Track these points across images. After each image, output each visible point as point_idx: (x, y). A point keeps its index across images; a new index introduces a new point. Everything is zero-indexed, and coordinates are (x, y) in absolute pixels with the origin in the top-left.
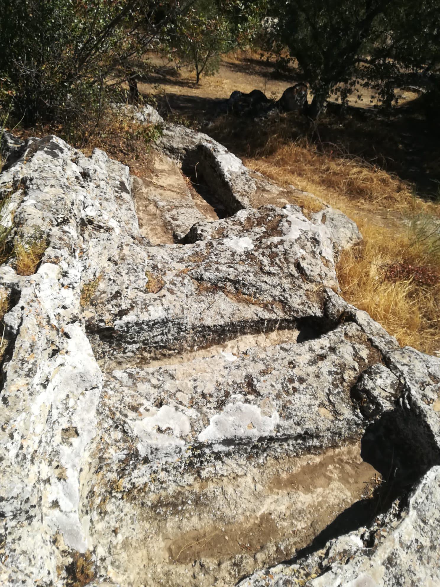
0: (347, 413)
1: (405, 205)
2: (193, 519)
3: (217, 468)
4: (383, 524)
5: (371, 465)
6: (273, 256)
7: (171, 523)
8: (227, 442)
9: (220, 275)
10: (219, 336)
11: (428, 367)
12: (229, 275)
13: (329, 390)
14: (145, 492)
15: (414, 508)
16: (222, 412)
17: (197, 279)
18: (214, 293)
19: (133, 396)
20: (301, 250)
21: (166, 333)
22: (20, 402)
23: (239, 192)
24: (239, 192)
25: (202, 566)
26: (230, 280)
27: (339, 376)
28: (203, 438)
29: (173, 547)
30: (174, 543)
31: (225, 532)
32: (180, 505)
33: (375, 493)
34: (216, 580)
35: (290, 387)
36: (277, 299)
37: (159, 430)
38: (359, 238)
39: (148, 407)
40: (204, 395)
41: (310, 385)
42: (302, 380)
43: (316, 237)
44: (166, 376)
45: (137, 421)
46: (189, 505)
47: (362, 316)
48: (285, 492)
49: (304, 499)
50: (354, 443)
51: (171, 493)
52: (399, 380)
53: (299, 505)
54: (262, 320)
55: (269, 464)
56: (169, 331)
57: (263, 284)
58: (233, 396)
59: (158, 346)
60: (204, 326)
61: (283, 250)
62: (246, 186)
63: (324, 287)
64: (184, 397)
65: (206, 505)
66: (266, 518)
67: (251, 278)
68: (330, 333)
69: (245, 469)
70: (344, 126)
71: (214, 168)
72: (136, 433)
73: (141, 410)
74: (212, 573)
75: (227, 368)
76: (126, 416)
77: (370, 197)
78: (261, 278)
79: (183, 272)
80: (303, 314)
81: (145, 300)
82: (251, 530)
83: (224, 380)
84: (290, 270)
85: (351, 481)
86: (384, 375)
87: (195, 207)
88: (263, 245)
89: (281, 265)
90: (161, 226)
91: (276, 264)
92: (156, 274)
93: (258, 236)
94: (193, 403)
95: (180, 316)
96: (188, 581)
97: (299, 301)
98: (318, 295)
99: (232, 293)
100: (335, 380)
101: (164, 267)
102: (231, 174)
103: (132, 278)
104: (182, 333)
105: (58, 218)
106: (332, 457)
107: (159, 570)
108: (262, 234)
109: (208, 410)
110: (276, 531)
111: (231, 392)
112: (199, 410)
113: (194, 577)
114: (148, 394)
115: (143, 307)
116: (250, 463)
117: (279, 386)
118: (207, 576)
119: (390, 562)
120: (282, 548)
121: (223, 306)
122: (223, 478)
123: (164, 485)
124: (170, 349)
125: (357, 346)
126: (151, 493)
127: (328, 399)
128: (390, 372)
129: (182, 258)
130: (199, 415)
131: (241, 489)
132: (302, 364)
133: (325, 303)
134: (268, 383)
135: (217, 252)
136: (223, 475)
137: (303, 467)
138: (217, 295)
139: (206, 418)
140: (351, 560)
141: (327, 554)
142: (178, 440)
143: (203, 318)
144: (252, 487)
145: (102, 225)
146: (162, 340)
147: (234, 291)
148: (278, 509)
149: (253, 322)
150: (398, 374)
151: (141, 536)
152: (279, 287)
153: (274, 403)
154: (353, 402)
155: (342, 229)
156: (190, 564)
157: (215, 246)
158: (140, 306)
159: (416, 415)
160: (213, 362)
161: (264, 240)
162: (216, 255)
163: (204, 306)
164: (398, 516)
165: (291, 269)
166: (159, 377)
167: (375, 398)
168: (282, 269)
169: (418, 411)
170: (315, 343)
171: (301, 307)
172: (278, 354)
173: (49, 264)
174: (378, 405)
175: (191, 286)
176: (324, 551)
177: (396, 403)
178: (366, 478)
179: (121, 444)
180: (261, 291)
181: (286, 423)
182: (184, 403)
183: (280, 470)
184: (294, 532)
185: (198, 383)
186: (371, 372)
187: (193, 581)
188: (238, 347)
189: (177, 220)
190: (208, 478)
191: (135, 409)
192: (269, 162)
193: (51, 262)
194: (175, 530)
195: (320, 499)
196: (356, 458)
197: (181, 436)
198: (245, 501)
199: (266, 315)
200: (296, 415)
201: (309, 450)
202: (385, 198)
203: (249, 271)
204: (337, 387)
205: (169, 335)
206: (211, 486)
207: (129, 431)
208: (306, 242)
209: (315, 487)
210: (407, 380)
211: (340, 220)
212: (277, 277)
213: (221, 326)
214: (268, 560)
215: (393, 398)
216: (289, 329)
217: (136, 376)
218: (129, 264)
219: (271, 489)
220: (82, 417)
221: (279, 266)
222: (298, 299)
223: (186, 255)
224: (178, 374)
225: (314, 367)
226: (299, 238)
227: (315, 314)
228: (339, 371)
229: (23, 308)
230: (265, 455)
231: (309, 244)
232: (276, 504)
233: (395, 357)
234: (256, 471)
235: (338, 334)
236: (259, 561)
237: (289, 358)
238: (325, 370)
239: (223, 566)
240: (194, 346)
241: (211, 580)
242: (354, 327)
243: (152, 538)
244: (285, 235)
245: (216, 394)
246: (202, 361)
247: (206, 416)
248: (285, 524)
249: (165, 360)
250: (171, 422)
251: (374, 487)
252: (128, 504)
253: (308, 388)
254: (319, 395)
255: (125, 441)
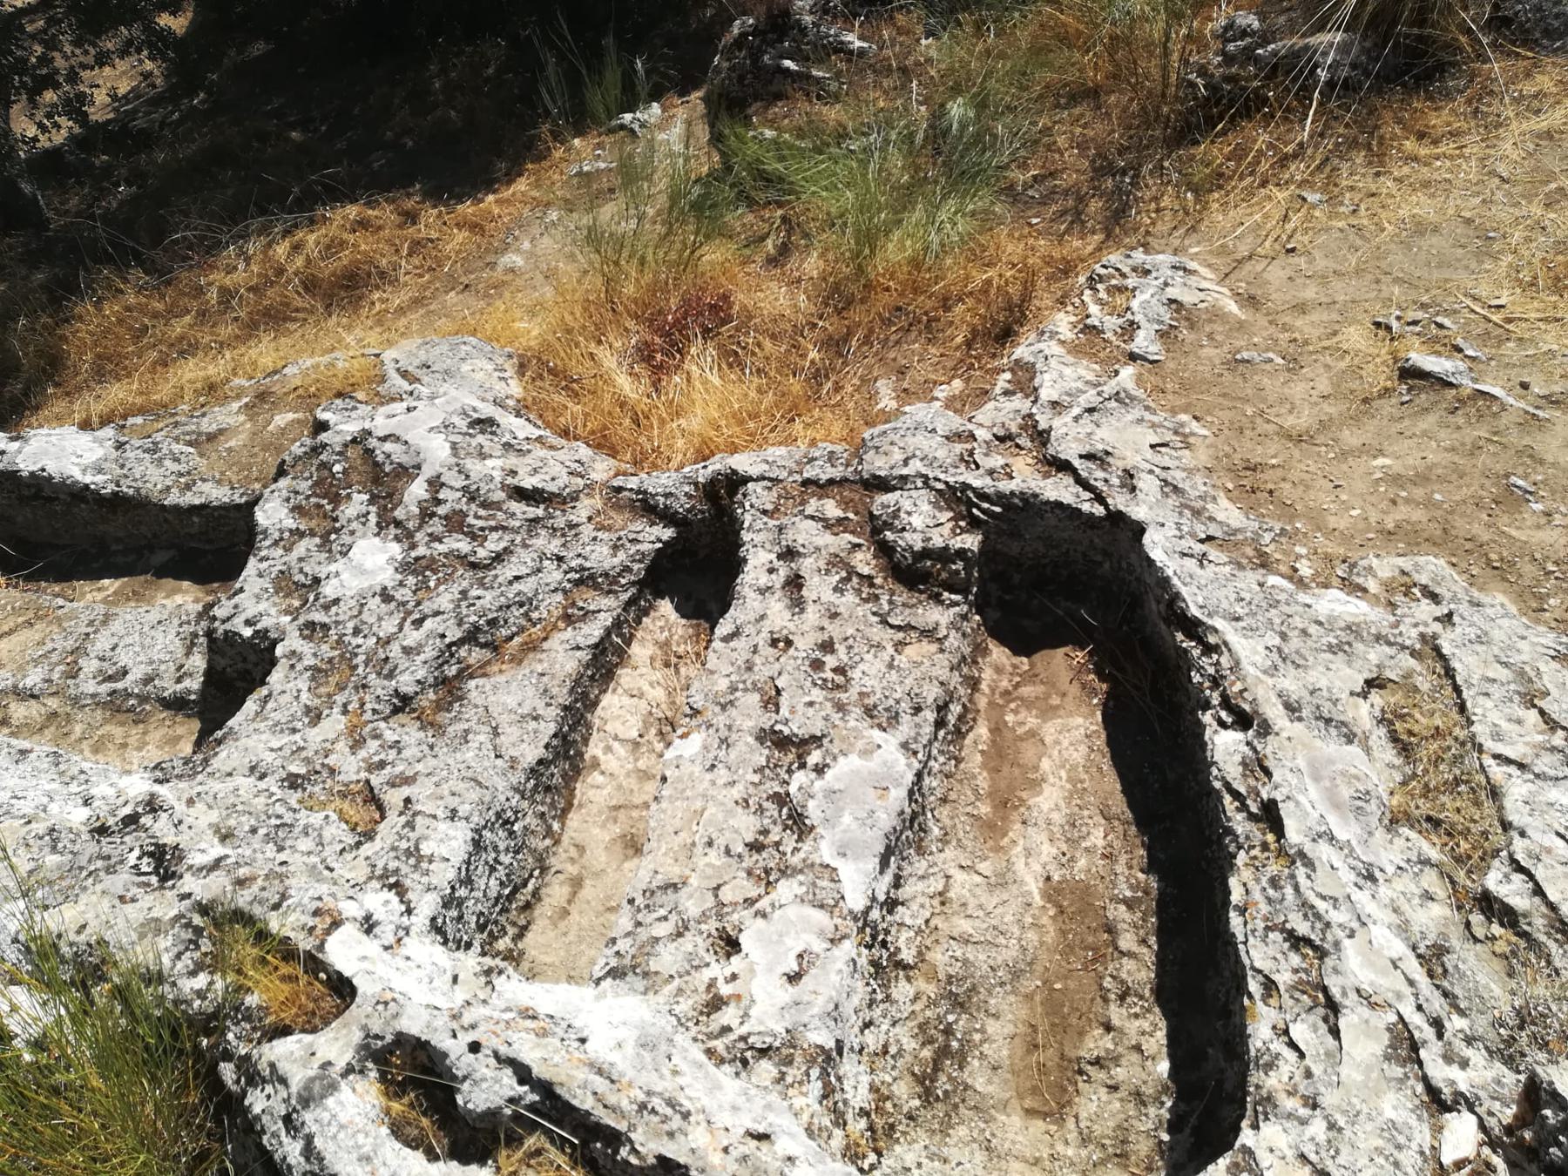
0: (937, 616)
1: (461, 236)
2: (990, 1030)
3: (908, 922)
4: (1216, 682)
5: (1044, 652)
6: (456, 522)
7: (978, 1077)
8: (884, 863)
9: (429, 653)
10: (567, 757)
11: (934, 431)
12: (443, 636)
13: (874, 614)
14: (888, 1098)
15: (1210, 615)
16: (819, 830)
17: (396, 711)
18: (461, 699)
19: (680, 991)
20: (490, 463)
21: (496, 860)
22: (758, 1158)
23: (168, 489)
24: (168, 489)
25: (1097, 1062)
26: (459, 643)
27: (855, 580)
28: (856, 902)
29: (1028, 1103)
30: (1021, 1097)
31: (1044, 983)
32: (947, 1040)
33: (1102, 677)
34: (1138, 1048)
35: (829, 675)
36: (569, 586)
37: (794, 978)
38: (510, 356)
39: (728, 973)
40: (756, 847)
41: (846, 639)
42: (828, 647)
43: (476, 416)
44: (660, 898)
45: (752, 1012)
46: (956, 1021)
47: (743, 463)
48: (1018, 826)
49: (1049, 801)
50: (987, 648)
51: (914, 1045)
52: (932, 489)
53: (1057, 817)
54: (596, 646)
55: (948, 822)
56: (496, 848)
57: (517, 587)
58: (793, 789)
59: (503, 902)
60: (532, 770)
61: (459, 494)
62: (168, 463)
63: (604, 484)
64: (739, 888)
65: (973, 989)
66: (1053, 891)
67: (489, 598)
68: (746, 536)
69: (936, 869)
70: (129, 184)
71: (37, 496)
72: (779, 1029)
73: (725, 990)
74: (1120, 1049)
75: (713, 766)
76: (726, 1030)
77: (382, 275)
78: (500, 579)
79: (352, 729)
80: (640, 561)
81: (394, 849)
82: (1064, 933)
83: (740, 787)
84: (520, 516)
85: (1055, 700)
86: (906, 505)
87: (114, 610)
88: (411, 525)
89: (493, 523)
90: (106, 721)
91: (482, 529)
92: (317, 789)
93: (373, 519)
94: (767, 880)
95: (487, 799)
96: (1118, 1105)
97: (606, 550)
98: (618, 507)
99: (488, 662)
100: (858, 592)
101: (307, 761)
102: (100, 471)
103: (305, 844)
104: (516, 828)
105: (136, 867)
106: (991, 704)
107: (1070, 1152)
108: (373, 509)
109: (802, 855)
110: (1088, 887)
111: (778, 789)
112: (786, 872)
113: (1114, 1088)
114: (690, 957)
115: (412, 861)
116: (931, 853)
117: (817, 695)
118: (1123, 1062)
119: (1292, 708)
120: (1128, 894)
121: (511, 701)
122: (932, 923)
123: (893, 1050)
124: (525, 885)
125: (809, 510)
126: (894, 1088)
127: (892, 627)
128: (905, 494)
129: (308, 710)
130: (801, 877)
131: (972, 903)
132: (791, 625)
133: (647, 507)
134: (800, 708)
135: (350, 625)
136: (927, 921)
137: (984, 766)
138: (473, 695)
139: (817, 868)
140: (1267, 763)
141: (1236, 795)
142: (836, 952)
143: (513, 760)
144: (978, 879)
145: (127, 810)
146: (502, 884)
147: (486, 654)
148: (1044, 858)
149: (587, 666)
150: (920, 484)
151: (980, 1157)
152: (546, 563)
153: (852, 723)
154: (921, 592)
155: (465, 368)
156: (1080, 1084)
157: (326, 620)
158: (405, 869)
159: (1022, 509)
160: (680, 786)
161: (399, 513)
162: (357, 631)
163: (482, 738)
164: (1209, 650)
165: (518, 512)
166: (656, 915)
167: (946, 548)
168: (504, 528)
169: (1016, 501)
170: (752, 575)
171: (621, 556)
172: (735, 654)
173: (330, 939)
174: (961, 553)
175: (409, 733)
176: (1227, 799)
177: (974, 524)
178: (1065, 676)
179: (793, 1073)
180: (530, 600)
181: (905, 728)
182: (753, 894)
183: (969, 809)
184: (1104, 856)
185: (721, 842)
186: (885, 522)
187: (1122, 1094)
188: (616, 738)
189: (125, 672)
190: (920, 953)
191: (716, 1004)
192: (79, 389)
193: (328, 932)
194: (996, 1079)
195: (1063, 774)
196: (1015, 667)
197: (832, 941)
198: (1000, 910)
199: (593, 631)
200: (898, 702)
201: (959, 734)
202: (410, 255)
203: (464, 593)
204: (877, 598)
205: (502, 858)
206: (938, 957)
207: (769, 1040)
208: (474, 442)
209: (1036, 768)
210: (942, 476)
211: (439, 353)
212: (519, 550)
213: (555, 736)
214: (1142, 932)
215: (962, 524)
216: (646, 612)
217: (627, 961)
218: (254, 831)
219: (998, 849)
220: (727, 1106)
221: (494, 529)
222: (598, 548)
223: (304, 696)
224: (673, 872)
225: (811, 609)
226: (454, 446)
227: (659, 540)
228: (844, 574)
229: (475, 1047)
230: (929, 815)
231: (480, 439)
232: (1034, 857)
233: (878, 464)
234: (950, 853)
235: (759, 525)
236: (1135, 948)
237: (762, 639)
238: (828, 596)
239: (1116, 1022)
240: (550, 827)
241: (1135, 1057)
242: (759, 490)
243: (993, 1135)
244: (418, 467)
245: (766, 821)
246: (664, 805)
247: (812, 865)
248: (1082, 863)
249: (537, 913)
250: (789, 942)
251: (1089, 672)
252: (897, 1148)
253: (851, 647)
254: (877, 639)
255: (789, 1061)
